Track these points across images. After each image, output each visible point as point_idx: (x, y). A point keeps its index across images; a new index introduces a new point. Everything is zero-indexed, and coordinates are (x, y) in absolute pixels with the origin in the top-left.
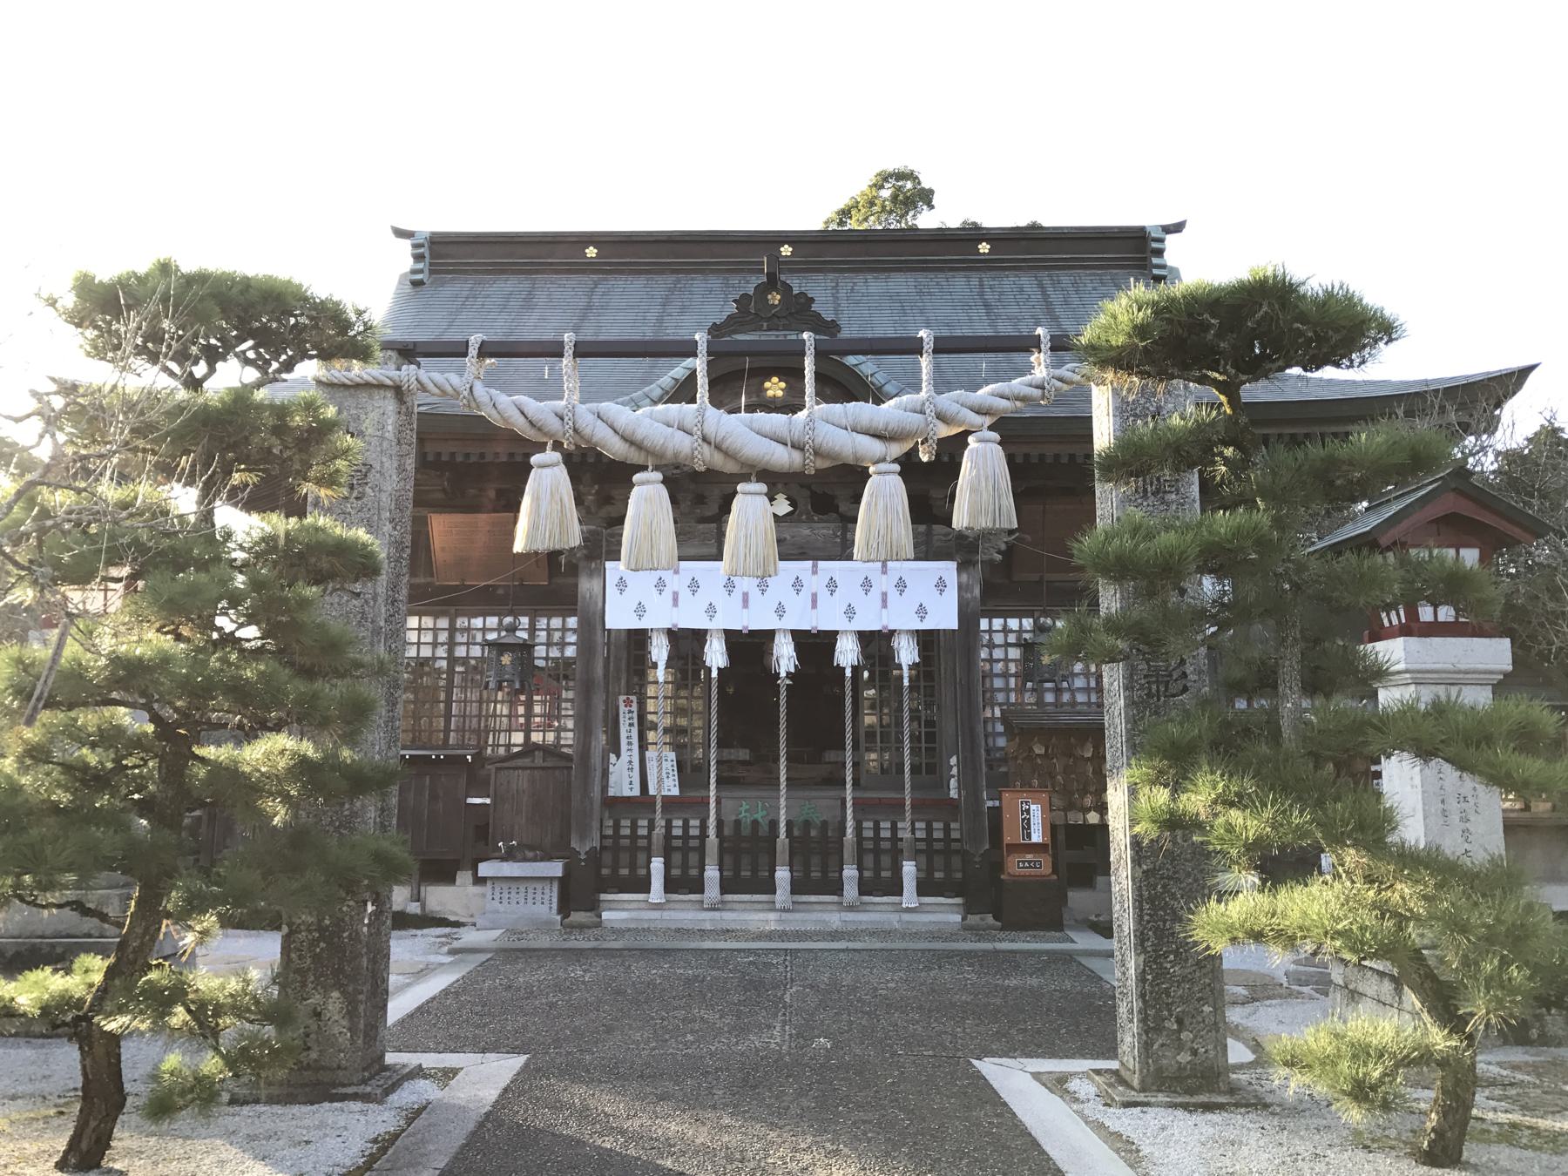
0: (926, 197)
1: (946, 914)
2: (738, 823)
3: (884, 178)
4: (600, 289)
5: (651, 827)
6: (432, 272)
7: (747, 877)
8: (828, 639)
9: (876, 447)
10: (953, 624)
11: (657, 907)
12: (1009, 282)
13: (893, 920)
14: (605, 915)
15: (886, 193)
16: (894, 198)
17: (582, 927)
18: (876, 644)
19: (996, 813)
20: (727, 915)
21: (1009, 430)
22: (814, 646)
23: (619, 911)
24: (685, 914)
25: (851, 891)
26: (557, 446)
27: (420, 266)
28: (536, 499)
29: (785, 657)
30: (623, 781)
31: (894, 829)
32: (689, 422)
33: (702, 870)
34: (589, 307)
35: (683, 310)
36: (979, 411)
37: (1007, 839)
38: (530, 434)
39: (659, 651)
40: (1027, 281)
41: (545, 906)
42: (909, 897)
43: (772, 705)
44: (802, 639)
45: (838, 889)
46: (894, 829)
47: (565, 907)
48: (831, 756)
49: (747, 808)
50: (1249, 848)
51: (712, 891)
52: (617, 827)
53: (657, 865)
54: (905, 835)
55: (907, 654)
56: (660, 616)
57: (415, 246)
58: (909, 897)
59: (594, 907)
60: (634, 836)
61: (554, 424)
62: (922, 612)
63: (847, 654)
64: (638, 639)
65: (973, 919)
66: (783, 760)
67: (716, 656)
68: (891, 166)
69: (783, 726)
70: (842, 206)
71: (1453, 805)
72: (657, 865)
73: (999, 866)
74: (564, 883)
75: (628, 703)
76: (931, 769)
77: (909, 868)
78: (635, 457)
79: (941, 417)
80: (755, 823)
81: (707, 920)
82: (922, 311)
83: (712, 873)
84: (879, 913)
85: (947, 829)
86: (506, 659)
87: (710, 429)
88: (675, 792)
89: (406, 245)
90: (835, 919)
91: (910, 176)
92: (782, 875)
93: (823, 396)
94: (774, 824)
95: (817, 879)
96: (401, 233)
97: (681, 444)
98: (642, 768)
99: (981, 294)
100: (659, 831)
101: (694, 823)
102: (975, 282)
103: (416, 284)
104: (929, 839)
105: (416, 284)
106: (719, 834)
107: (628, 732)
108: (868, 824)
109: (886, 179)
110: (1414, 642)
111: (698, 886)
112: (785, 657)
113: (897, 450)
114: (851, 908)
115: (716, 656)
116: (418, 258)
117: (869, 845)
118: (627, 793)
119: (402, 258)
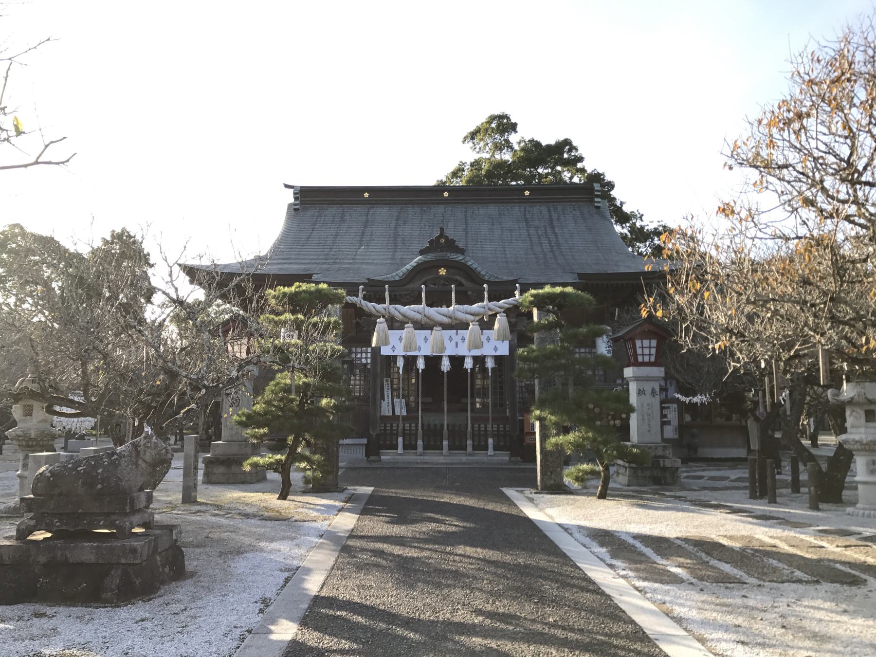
0: (513, 127)
1: (504, 457)
2: (429, 425)
3: (492, 118)
4: (371, 212)
5: (398, 426)
6: (302, 204)
7: (433, 442)
8: (462, 359)
9: (472, 318)
10: (507, 353)
11: (401, 455)
12: (536, 209)
13: (485, 459)
14: (382, 457)
15: (493, 125)
16: (498, 126)
17: (374, 461)
18: (479, 360)
19: (522, 421)
20: (426, 458)
21: (508, 312)
22: (456, 361)
23: (387, 456)
24: (411, 457)
25: (470, 449)
26: (384, 317)
27: (297, 202)
28: (378, 332)
29: (446, 365)
30: (386, 409)
31: (486, 427)
32: (421, 311)
33: (416, 442)
34: (367, 221)
35: (405, 223)
36: (500, 307)
37: (526, 430)
38: (377, 314)
39: (400, 363)
40: (544, 209)
41: (361, 454)
42: (490, 451)
43: (441, 383)
44: (452, 358)
45: (465, 448)
46: (486, 427)
47: (367, 455)
48: (463, 400)
49: (433, 419)
50: (554, 424)
51: (420, 449)
52: (385, 426)
53: (400, 439)
54: (489, 428)
55: (490, 364)
56: (400, 351)
57: (295, 194)
58: (490, 451)
59: (378, 454)
60: (391, 429)
61: (384, 311)
62: (496, 349)
63: (468, 364)
64: (392, 359)
65: (513, 459)
66: (445, 402)
67: (421, 365)
68: (497, 112)
69: (445, 390)
70: (472, 130)
71: (646, 417)
72: (400, 439)
73: (523, 440)
74: (367, 446)
75: (387, 381)
76: (501, 405)
77: (490, 441)
78: (406, 320)
79: (490, 309)
80: (435, 425)
81: (419, 459)
82: (500, 223)
83: (420, 443)
84: (480, 457)
85: (505, 428)
86: (345, 366)
87: (426, 313)
88: (405, 414)
89: (292, 191)
90: (464, 459)
91: (506, 117)
92: (445, 443)
93: (458, 302)
94: (442, 425)
95: (457, 445)
96: (287, 186)
97: (418, 317)
98: (392, 405)
99: (525, 215)
100: (401, 427)
101: (413, 425)
102: (522, 209)
103: (295, 210)
104: (498, 431)
105: (295, 210)
106: (422, 428)
107: (387, 392)
108: (476, 426)
109: (494, 119)
110: (636, 368)
111: (415, 447)
112: (446, 365)
113: (477, 318)
114: (470, 455)
115: (421, 365)
116: (296, 199)
117: (476, 433)
118: (387, 414)
119: (289, 197)
